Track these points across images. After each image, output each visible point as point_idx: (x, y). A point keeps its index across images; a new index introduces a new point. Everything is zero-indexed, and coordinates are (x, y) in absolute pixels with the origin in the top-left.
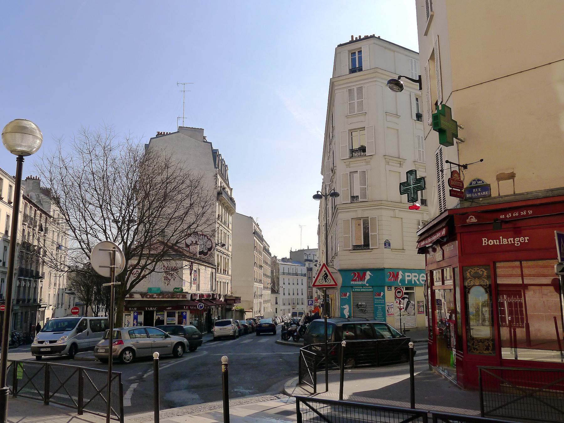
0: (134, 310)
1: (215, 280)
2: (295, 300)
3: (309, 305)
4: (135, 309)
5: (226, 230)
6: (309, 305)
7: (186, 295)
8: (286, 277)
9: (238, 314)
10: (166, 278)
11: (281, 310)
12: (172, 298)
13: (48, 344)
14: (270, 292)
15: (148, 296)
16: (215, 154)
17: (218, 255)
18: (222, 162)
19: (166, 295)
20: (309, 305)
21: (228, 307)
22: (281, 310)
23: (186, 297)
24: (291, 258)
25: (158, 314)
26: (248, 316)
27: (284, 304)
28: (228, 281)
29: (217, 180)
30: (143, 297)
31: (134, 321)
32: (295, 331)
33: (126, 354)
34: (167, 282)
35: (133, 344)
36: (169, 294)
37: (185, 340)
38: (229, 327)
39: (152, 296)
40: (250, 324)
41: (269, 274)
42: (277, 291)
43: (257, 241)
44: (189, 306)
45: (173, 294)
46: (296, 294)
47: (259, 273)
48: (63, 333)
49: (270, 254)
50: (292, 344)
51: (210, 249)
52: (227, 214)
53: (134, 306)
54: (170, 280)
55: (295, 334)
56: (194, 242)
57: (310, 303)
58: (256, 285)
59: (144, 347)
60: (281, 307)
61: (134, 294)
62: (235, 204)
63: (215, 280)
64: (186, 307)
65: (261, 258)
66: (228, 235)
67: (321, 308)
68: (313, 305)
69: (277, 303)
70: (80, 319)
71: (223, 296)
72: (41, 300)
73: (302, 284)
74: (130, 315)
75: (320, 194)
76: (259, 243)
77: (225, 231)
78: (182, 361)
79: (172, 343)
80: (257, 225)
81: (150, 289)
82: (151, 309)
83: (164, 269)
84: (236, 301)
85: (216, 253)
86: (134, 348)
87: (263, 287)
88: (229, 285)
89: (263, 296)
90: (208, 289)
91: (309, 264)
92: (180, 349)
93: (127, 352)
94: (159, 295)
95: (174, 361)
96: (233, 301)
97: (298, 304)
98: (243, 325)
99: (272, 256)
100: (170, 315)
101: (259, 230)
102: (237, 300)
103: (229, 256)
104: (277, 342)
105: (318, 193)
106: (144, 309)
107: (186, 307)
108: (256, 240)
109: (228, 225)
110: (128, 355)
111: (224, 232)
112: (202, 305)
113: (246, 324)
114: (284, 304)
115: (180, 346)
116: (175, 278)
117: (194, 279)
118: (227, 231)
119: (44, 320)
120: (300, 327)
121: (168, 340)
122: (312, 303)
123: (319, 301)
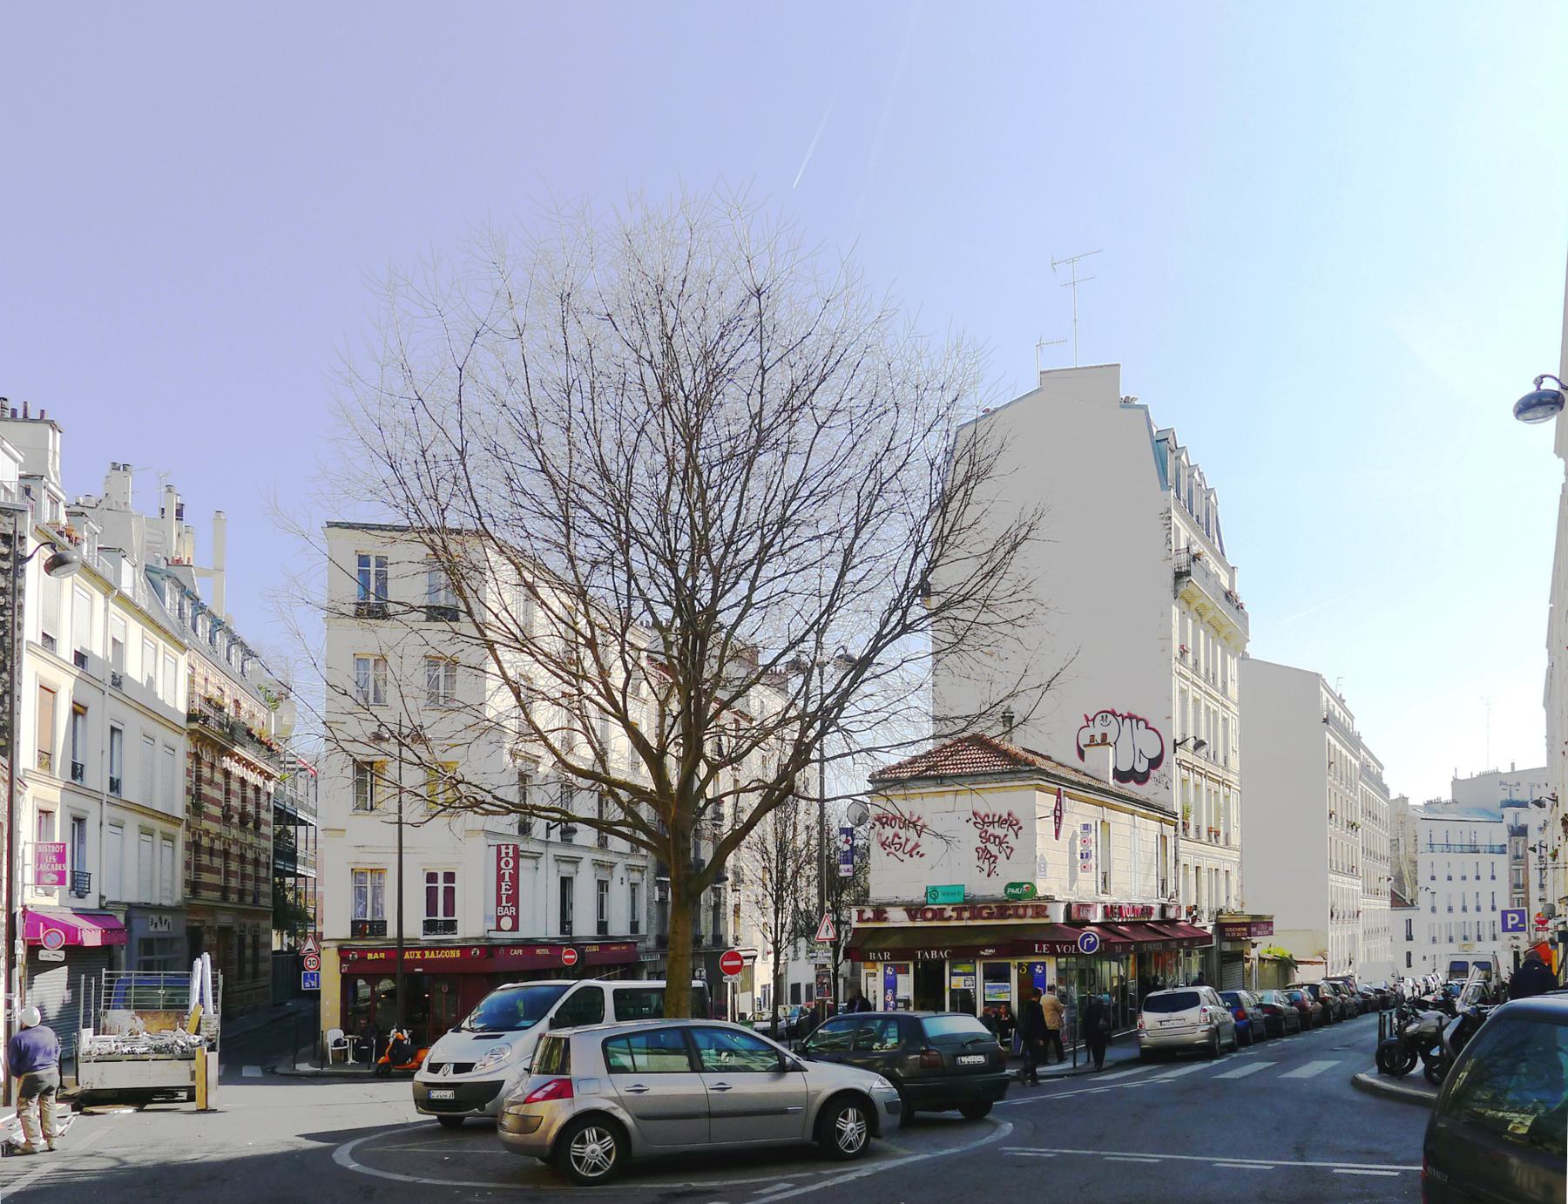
0: (883, 960)
1: (1177, 861)
2: (1470, 926)
3: (1505, 929)
4: (887, 955)
5: (1217, 701)
6: (1505, 929)
7: (1045, 907)
8: (1440, 858)
9: (1270, 969)
10: (984, 854)
11: (1425, 958)
12: (1002, 916)
13: (452, 1078)
14: (1388, 903)
15: (929, 915)
16: (1163, 447)
17: (1184, 781)
18: (1191, 476)
19: (984, 908)
20: (1509, 931)
21: (1227, 947)
22: (1425, 958)
23: (1048, 913)
24: (1455, 801)
25: (955, 971)
26: (1303, 975)
27: (1434, 940)
28: (1227, 866)
29: (1170, 528)
30: (912, 918)
31: (885, 994)
32: (1435, 1038)
33: (582, 1140)
34: (986, 867)
35: (619, 1101)
36: (993, 906)
37: (874, 1084)
38: (1191, 1015)
39: (938, 914)
40: (1291, 1004)
41: (1385, 850)
42: (1412, 901)
43: (1338, 746)
44: (1052, 944)
45: (1002, 908)
46: (1471, 907)
47: (1339, 844)
48: (498, 1037)
49: (1386, 791)
50: (1420, 1097)
51: (1155, 763)
52: (1219, 648)
53: (883, 945)
54: (996, 858)
55: (1435, 1052)
56: (1098, 739)
57: (1510, 923)
58: (1337, 882)
59: (681, 1110)
60: (1419, 947)
61: (888, 909)
62: (1246, 617)
63: (1177, 861)
64: (1040, 948)
65: (1353, 799)
66: (1225, 719)
67: (1561, 945)
68: (1523, 929)
69: (1409, 938)
70: (571, 986)
71: (1211, 914)
72: (736, 939)
73: (1493, 878)
74: (875, 975)
75: (1555, 387)
76: (1345, 752)
77: (1209, 704)
78: (852, 1177)
79: (808, 1097)
80: (1341, 701)
81: (932, 892)
82: (934, 954)
83: (975, 823)
84: (1254, 929)
85: (1177, 774)
86: (627, 1119)
87: (1360, 888)
88: (1234, 878)
89: (1360, 914)
90: (1148, 888)
91: (1516, 815)
92: (850, 1126)
93: (590, 1134)
94: (959, 910)
95: (786, 1181)
96: (1245, 929)
97: (1479, 939)
98: (1260, 1006)
99: (1394, 795)
100: (997, 974)
101: (1343, 713)
102: (1261, 924)
103: (1229, 787)
104: (1357, 1084)
105: (1543, 387)
106: (912, 957)
107: (1040, 948)
108: (1333, 741)
109: (1225, 684)
110: (594, 1148)
111: (1207, 708)
112: (1092, 939)
113: (1274, 1004)
114: (1434, 940)
115: (853, 1107)
116: (1012, 850)
117: (1082, 854)
118: (1189, 683)
119: (752, 990)
120: (1456, 1021)
121: (792, 1084)
122: (1522, 920)
123: (1550, 924)
